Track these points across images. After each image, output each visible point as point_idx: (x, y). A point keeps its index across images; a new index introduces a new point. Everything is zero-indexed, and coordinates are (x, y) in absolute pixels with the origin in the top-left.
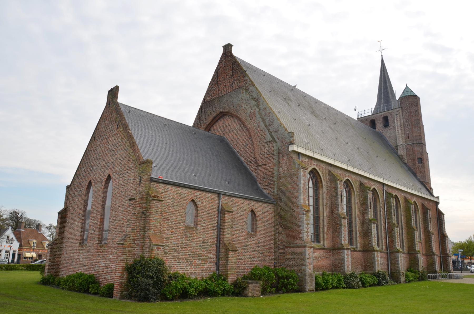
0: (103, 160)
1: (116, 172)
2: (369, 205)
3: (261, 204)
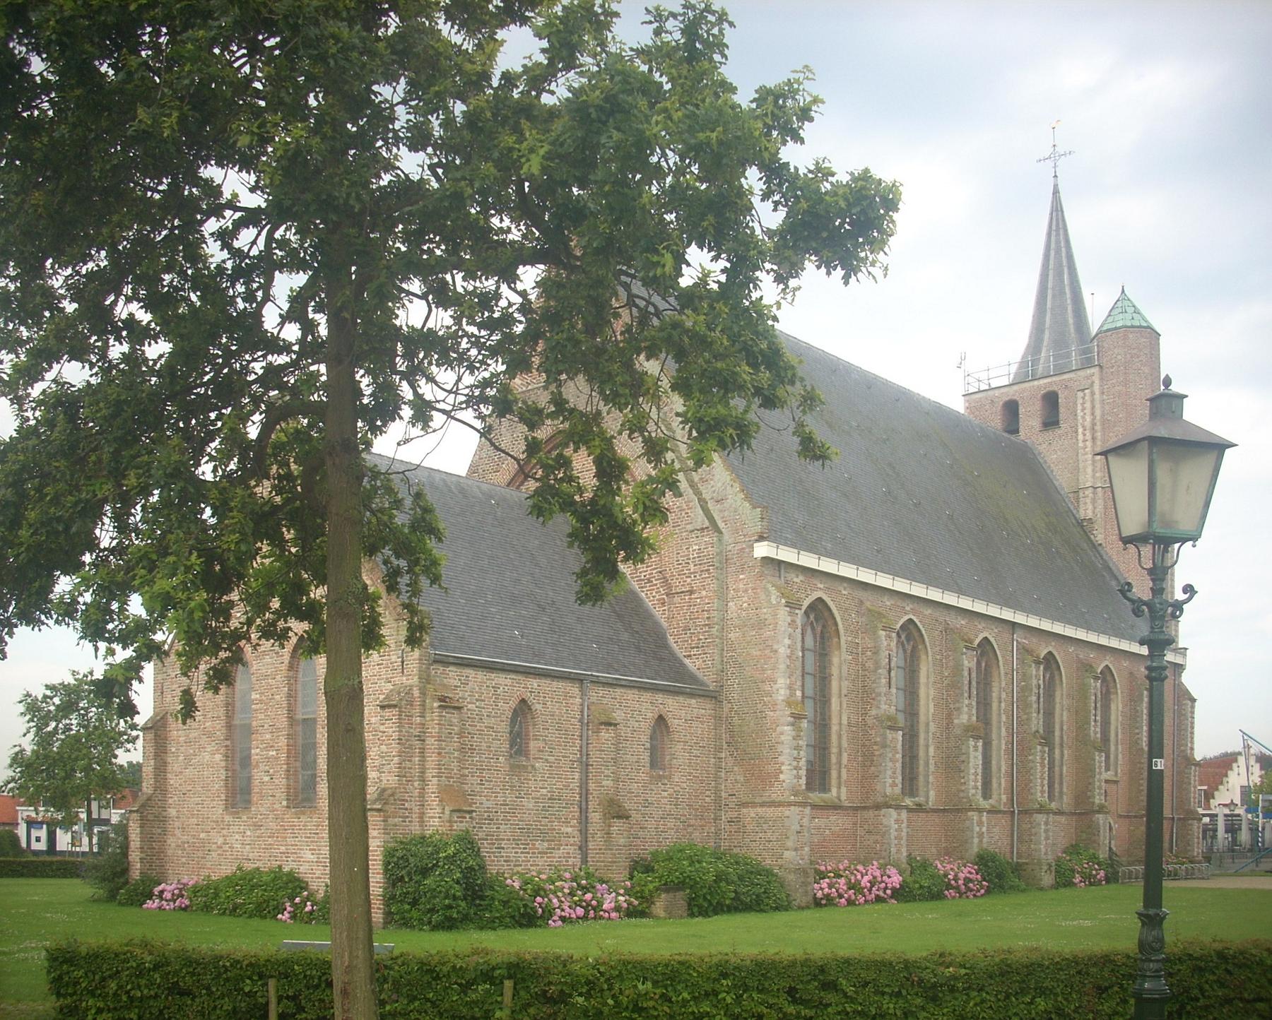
2: (966, 688)
3: (681, 699)
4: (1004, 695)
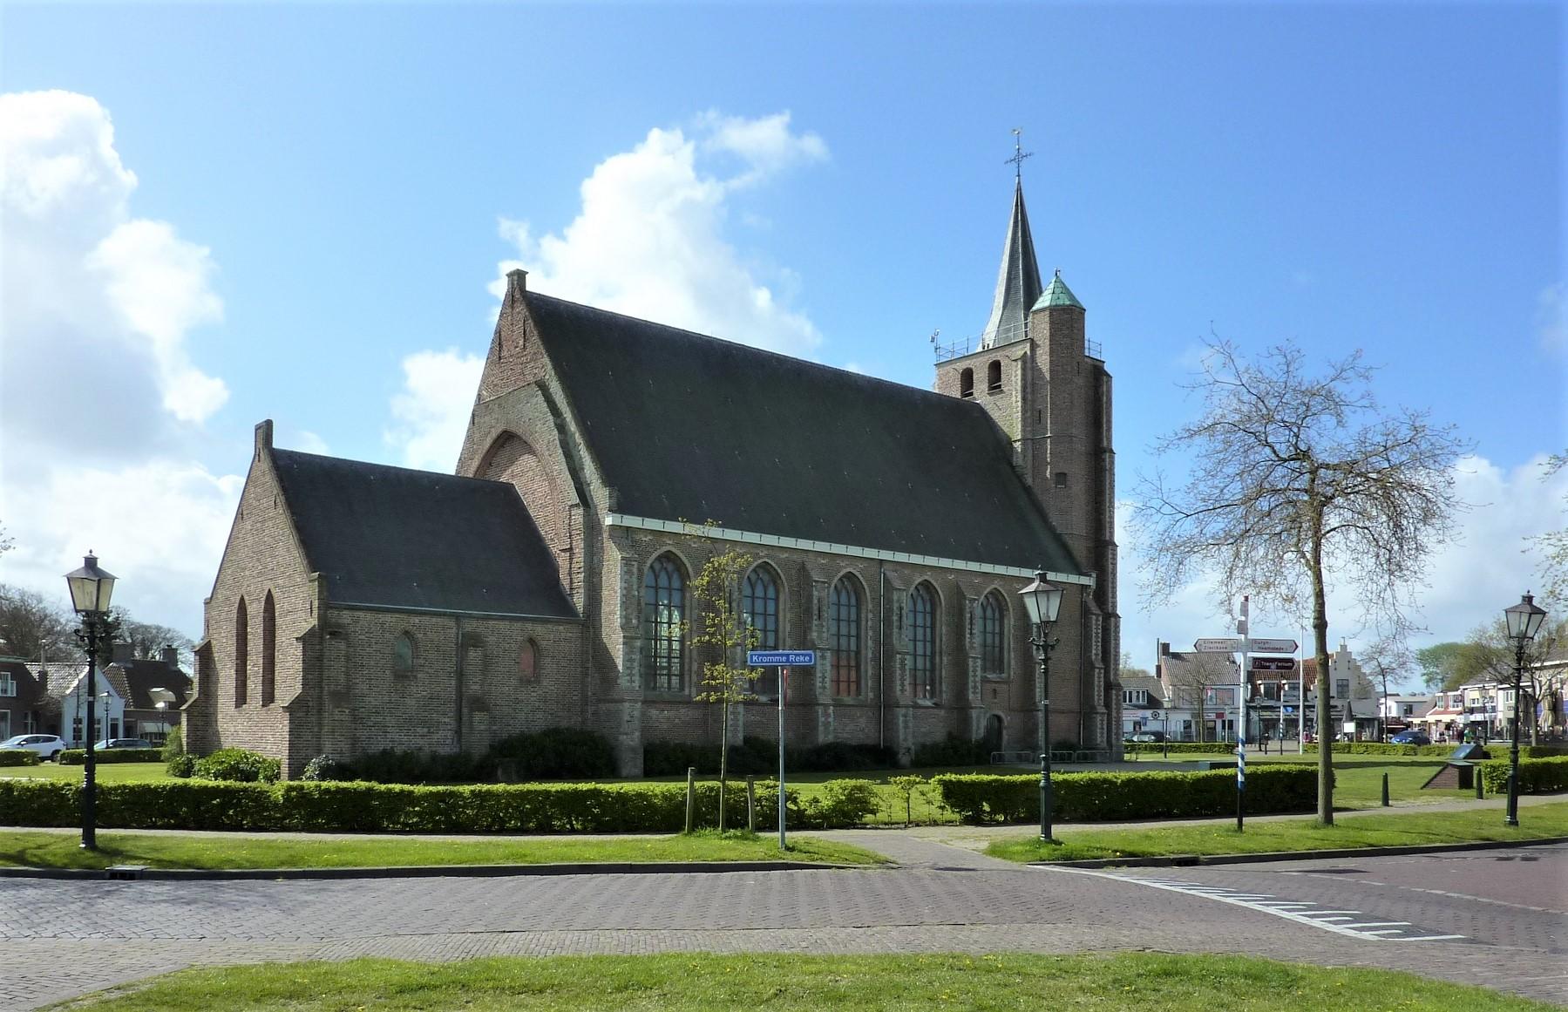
1: (277, 586)
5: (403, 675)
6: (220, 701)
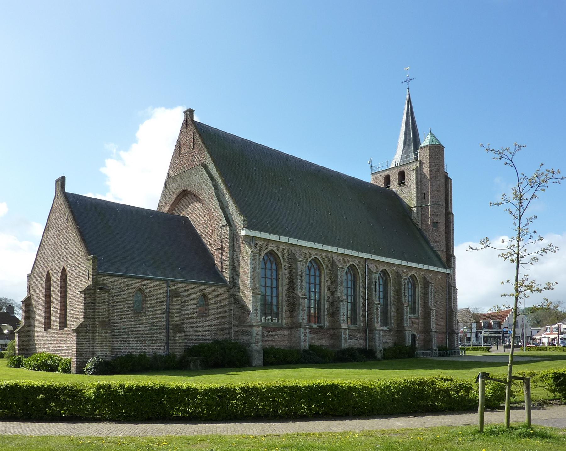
0: (57, 251)
1: (69, 264)
4: (361, 286)
5: (139, 311)
6: (36, 327)
